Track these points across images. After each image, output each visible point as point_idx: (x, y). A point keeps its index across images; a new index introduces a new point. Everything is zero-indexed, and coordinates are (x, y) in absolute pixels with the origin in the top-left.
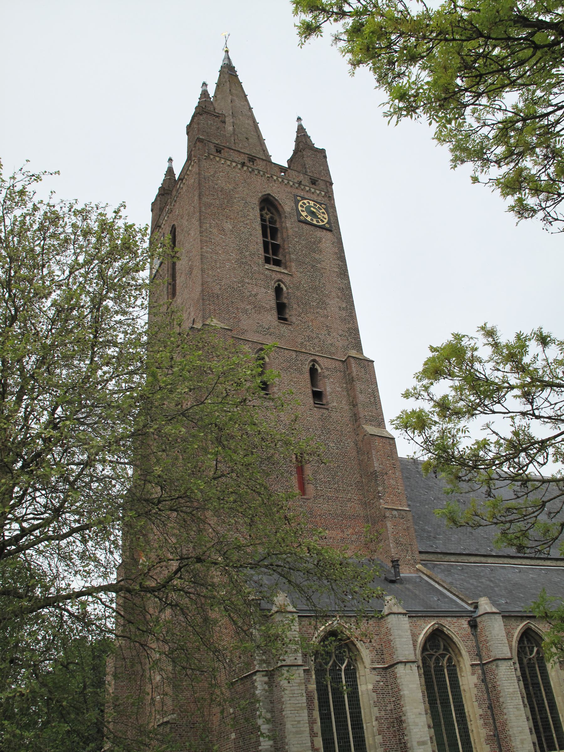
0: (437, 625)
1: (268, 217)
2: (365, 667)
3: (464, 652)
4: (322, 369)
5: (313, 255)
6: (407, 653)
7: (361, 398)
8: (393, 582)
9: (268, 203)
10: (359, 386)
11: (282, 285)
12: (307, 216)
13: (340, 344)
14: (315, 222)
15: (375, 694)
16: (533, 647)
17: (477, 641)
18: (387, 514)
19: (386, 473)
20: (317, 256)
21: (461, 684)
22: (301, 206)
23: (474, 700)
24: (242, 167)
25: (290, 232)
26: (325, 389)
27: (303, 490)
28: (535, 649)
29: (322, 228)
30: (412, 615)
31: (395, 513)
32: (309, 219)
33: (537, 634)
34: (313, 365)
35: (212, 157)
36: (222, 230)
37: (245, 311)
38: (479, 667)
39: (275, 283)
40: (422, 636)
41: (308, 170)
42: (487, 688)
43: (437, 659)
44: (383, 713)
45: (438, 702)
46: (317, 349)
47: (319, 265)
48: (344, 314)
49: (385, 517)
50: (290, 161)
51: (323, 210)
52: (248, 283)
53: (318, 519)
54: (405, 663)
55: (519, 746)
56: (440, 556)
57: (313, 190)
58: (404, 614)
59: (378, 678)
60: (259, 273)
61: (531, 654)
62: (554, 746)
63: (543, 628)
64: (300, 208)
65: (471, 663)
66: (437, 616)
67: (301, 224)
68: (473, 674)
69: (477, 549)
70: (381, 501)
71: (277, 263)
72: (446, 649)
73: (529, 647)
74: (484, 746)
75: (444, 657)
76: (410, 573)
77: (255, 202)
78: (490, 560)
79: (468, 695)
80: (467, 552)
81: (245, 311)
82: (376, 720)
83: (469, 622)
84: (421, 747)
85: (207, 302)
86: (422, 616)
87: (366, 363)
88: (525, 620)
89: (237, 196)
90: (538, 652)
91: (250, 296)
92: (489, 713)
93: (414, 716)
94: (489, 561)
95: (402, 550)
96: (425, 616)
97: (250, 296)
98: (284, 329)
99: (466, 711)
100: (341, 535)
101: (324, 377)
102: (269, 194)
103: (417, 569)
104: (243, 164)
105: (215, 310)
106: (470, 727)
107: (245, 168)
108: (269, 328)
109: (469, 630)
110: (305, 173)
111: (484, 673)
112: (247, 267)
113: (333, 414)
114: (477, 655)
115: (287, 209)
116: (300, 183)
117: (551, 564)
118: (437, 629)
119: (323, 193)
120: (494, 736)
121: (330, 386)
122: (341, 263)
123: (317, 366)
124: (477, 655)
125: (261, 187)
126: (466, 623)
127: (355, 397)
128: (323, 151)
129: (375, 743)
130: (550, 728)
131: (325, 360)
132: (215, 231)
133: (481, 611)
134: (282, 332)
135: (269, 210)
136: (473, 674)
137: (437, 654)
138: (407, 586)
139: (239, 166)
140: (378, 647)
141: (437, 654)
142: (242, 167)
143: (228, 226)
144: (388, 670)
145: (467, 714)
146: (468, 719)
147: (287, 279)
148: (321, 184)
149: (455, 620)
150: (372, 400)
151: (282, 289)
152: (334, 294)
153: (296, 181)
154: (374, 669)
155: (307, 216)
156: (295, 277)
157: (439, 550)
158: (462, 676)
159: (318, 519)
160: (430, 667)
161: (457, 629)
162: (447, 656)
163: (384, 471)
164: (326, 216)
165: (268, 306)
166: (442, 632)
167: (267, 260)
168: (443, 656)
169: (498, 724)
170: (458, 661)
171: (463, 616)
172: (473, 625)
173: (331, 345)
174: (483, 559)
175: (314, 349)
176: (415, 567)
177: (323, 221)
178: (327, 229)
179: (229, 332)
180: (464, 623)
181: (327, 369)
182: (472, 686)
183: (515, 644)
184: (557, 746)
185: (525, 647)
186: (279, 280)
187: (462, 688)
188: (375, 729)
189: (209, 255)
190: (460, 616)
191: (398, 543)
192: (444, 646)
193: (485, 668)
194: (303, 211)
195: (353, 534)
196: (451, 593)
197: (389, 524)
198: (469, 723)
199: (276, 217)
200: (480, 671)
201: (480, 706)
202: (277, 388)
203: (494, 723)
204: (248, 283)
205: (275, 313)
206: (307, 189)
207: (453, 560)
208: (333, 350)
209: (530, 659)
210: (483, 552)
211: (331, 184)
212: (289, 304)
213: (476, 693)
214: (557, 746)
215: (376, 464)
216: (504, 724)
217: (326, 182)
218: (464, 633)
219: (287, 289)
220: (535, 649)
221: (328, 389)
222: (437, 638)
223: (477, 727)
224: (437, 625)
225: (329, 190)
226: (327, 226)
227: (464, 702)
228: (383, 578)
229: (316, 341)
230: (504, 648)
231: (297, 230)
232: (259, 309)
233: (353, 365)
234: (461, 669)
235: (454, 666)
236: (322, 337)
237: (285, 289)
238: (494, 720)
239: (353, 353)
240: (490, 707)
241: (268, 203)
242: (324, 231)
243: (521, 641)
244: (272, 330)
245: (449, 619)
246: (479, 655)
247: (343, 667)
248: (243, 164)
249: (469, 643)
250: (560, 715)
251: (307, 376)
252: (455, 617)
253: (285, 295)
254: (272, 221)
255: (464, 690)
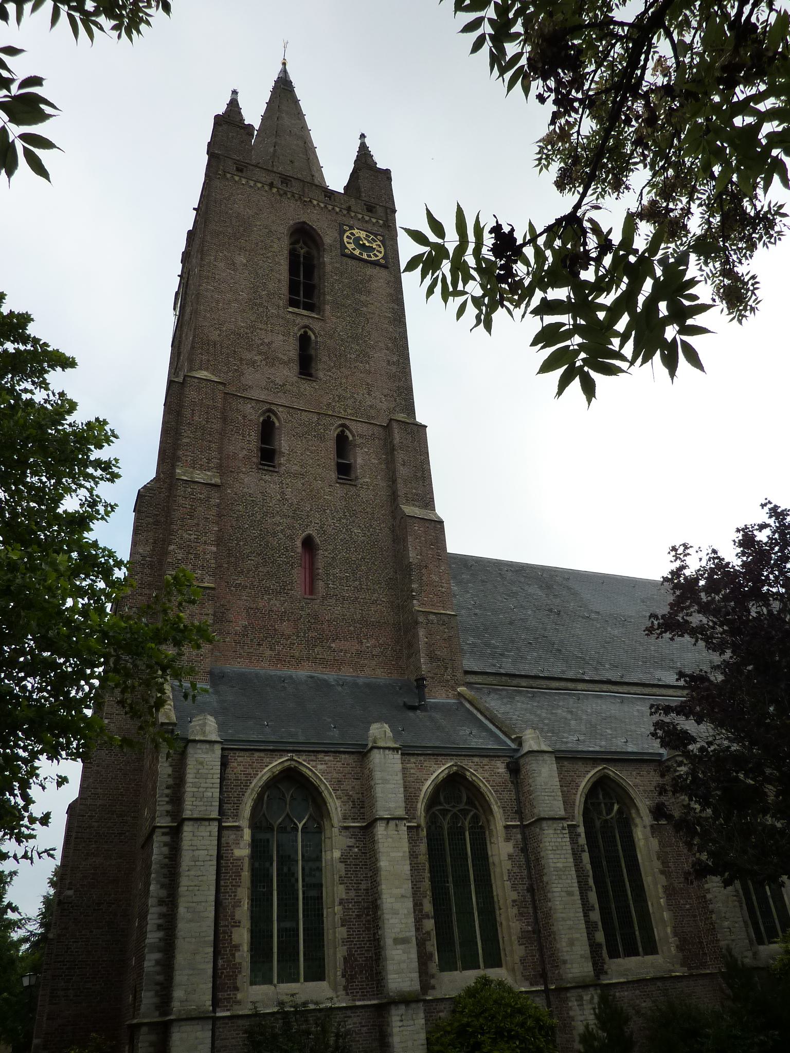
0: (455, 768)
1: (302, 251)
2: (333, 826)
3: (495, 808)
4: (353, 436)
5: (357, 296)
6: (392, 805)
7: (403, 471)
8: (413, 708)
9: (303, 235)
10: (400, 456)
11: (310, 333)
12: (354, 249)
13: (384, 406)
14: (365, 256)
15: (343, 865)
16: (613, 805)
17: (517, 793)
18: (421, 619)
19: (426, 567)
20: (363, 298)
21: (490, 853)
22: (348, 237)
23: (506, 878)
24: (271, 189)
25: (328, 268)
26: (355, 461)
27: (312, 589)
28: (616, 807)
29: (375, 264)
30: (406, 752)
31: (432, 617)
32: (357, 252)
33: (619, 785)
34: (343, 432)
35: (229, 176)
36: (233, 265)
37: (253, 363)
38: (518, 830)
39: (299, 330)
40: (429, 782)
41: (363, 195)
42: (528, 861)
43: (455, 816)
44: (352, 894)
45: (450, 879)
46: (349, 411)
47: (365, 309)
48: (394, 369)
49: (417, 623)
50: (346, 188)
51: (379, 243)
52: (261, 329)
53: (325, 626)
54: (388, 820)
55: (565, 949)
56: (504, 679)
57: (367, 218)
58: (393, 749)
59: (351, 842)
60: (278, 316)
61: (608, 814)
62: (637, 949)
63: (629, 779)
64: (346, 240)
65: (504, 824)
66: (457, 755)
67: (345, 259)
68: (508, 839)
69: (563, 672)
70: (415, 602)
71: (310, 307)
72: (470, 802)
73: (605, 804)
74: (516, 946)
75: (465, 816)
76: (448, 697)
77: (283, 229)
78: (580, 686)
79: (498, 870)
80: (546, 674)
81: (253, 363)
82: (340, 904)
83: (508, 764)
84: (399, 947)
85: (199, 351)
86: (433, 755)
87: (415, 428)
88: (599, 764)
89: (258, 223)
90: (620, 811)
91: (262, 344)
92: (528, 897)
93: (393, 900)
94: (579, 688)
95: (438, 666)
96: (437, 755)
97: (262, 344)
98: (306, 387)
99: (495, 894)
100: (358, 647)
101: (355, 446)
102: (304, 223)
103: (459, 693)
104: (271, 185)
105: (208, 361)
106: (498, 919)
107: (275, 190)
108: (284, 385)
109: (507, 776)
110: (358, 198)
111: (524, 839)
112: (261, 310)
113: (362, 493)
114: (516, 812)
115: (328, 240)
116: (349, 209)
117: (675, 694)
118: (455, 774)
119: (381, 222)
120: (534, 932)
121: (364, 459)
122: (396, 307)
123: (347, 433)
124: (516, 812)
125: (293, 213)
126: (503, 765)
127: (394, 472)
128: (387, 172)
129: (335, 937)
130: (631, 922)
131: (359, 424)
132: (221, 265)
133: (526, 749)
134: (302, 390)
135: (305, 243)
136: (508, 839)
137: (455, 810)
138: (434, 714)
139: (267, 188)
140: (356, 796)
141: (455, 810)
142: (271, 189)
143: (241, 259)
144: (365, 832)
145: (495, 899)
146: (497, 907)
147: (316, 326)
148: (380, 210)
149: (485, 761)
150: (419, 474)
151: (310, 337)
152: (381, 345)
153: (343, 206)
154: (346, 828)
155: (354, 249)
156: (329, 325)
157: (502, 671)
158: (491, 843)
159: (325, 626)
160: (441, 827)
161: (487, 776)
162: (472, 813)
163: (424, 564)
164: (382, 250)
165: (285, 358)
166: (464, 777)
167: (293, 303)
168: (465, 812)
169: (540, 915)
170: (488, 821)
171: (499, 757)
172: (515, 769)
173: (371, 407)
174: (570, 685)
175: (345, 411)
176: (456, 690)
177: (377, 256)
178: (381, 266)
179: (221, 387)
180: (500, 767)
181: (361, 436)
182: (504, 857)
183: (579, 799)
184: (641, 949)
185: (599, 804)
186: (306, 327)
187: (491, 860)
188: (337, 917)
189: (209, 294)
190: (495, 756)
191: (432, 658)
192: (468, 798)
193: (527, 831)
194: (348, 243)
195: (375, 646)
196: (494, 725)
197: (421, 633)
198: (497, 912)
199: (315, 253)
200: (519, 836)
201: (514, 888)
202: (285, 458)
203: (535, 912)
204: (261, 329)
205: (295, 368)
206: (360, 216)
207: (524, 684)
208: (373, 412)
209: (606, 821)
210: (571, 675)
211: (394, 211)
212: (316, 356)
213: (509, 867)
214: (641, 949)
215: (412, 554)
216: (548, 915)
217: (386, 208)
218: (498, 780)
219: (316, 337)
220: (616, 807)
221: (359, 461)
222: (455, 786)
223: (508, 920)
224: (455, 768)
225: (389, 218)
226: (383, 261)
227: (493, 881)
228: (402, 704)
229: (350, 402)
230: (555, 802)
231: (338, 265)
232: (271, 360)
233: (396, 431)
234: (491, 831)
235: (482, 827)
236: (359, 397)
237: (313, 337)
238: (535, 908)
239: (401, 417)
240: (531, 890)
241: (303, 235)
242: (378, 268)
243: (591, 793)
244: (288, 387)
245: (476, 759)
246: (520, 813)
247: (300, 826)
248: (271, 185)
249: (506, 795)
250: (650, 904)
251: (331, 445)
252: (487, 756)
253: (313, 345)
254: (309, 257)
255: (494, 864)
